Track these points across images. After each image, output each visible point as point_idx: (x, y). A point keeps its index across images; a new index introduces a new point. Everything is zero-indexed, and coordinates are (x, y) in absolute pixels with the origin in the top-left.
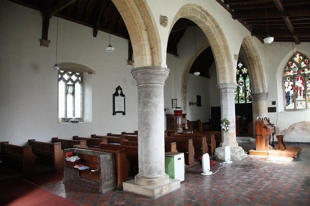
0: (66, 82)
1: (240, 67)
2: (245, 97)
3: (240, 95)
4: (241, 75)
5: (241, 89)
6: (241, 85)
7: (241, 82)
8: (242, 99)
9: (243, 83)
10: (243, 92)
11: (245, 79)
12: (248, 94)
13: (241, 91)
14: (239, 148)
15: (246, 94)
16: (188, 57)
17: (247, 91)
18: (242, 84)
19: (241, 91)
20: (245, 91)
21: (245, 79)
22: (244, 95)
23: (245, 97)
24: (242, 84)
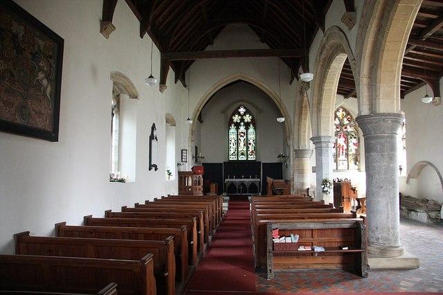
0: (237, 125)
3: (239, 150)
4: (242, 124)
6: (241, 136)
7: (242, 133)
8: (242, 154)
11: (247, 129)
13: (242, 144)
15: (248, 148)
17: (250, 144)
18: (243, 135)
19: (242, 144)
20: (247, 144)
21: (247, 129)
22: (245, 149)
24: (243, 135)
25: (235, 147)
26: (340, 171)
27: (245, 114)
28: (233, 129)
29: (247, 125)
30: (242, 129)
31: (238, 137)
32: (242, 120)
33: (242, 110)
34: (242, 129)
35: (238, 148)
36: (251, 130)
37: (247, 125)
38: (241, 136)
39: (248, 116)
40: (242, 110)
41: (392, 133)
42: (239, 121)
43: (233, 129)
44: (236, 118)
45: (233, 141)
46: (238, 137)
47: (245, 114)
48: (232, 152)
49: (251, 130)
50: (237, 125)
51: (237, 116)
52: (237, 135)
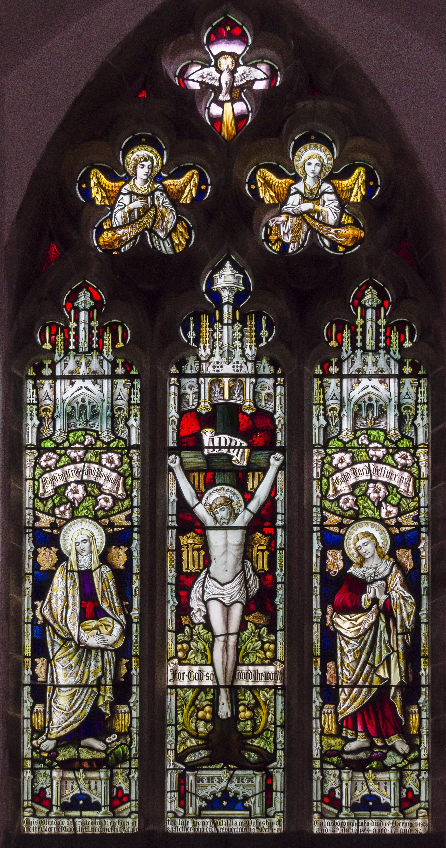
0: (152, 305)
1: (227, 112)
2: (298, 725)
3: (184, 674)
5: (225, 545)
7: (226, 417)
8: (226, 745)
9: (255, 428)
10: (258, 603)
11: (299, 352)
12: (347, 664)
13: (219, 594)
14: (94, 676)
15: (308, 655)
16: (72, 581)
17: (346, 591)
18: (239, 452)
19: (219, 594)
20: (296, 587)
21: (299, 352)
22: (265, 673)
23: (298, 725)
25: (107, 633)
26: (67, 574)
27: (274, 125)
28: (79, 384)
29: (302, 305)
30: (226, 360)
31: (153, 479)
32: (227, 218)
33: (226, 74)
34: (226, 360)
35: (154, 657)
36: (368, 383)
37: (302, 305)
38: (213, 471)
39: (312, 159)
40: (226, 74)
41: (83, 407)
42: (173, 238)
43: (79, 384)
44: (137, 195)
45: (81, 537)
46: (153, 479)
47: (274, 125)
48: (63, 712)
49: (368, 383)
50: (152, 305)
51: (142, 161)
52: (154, 451)
